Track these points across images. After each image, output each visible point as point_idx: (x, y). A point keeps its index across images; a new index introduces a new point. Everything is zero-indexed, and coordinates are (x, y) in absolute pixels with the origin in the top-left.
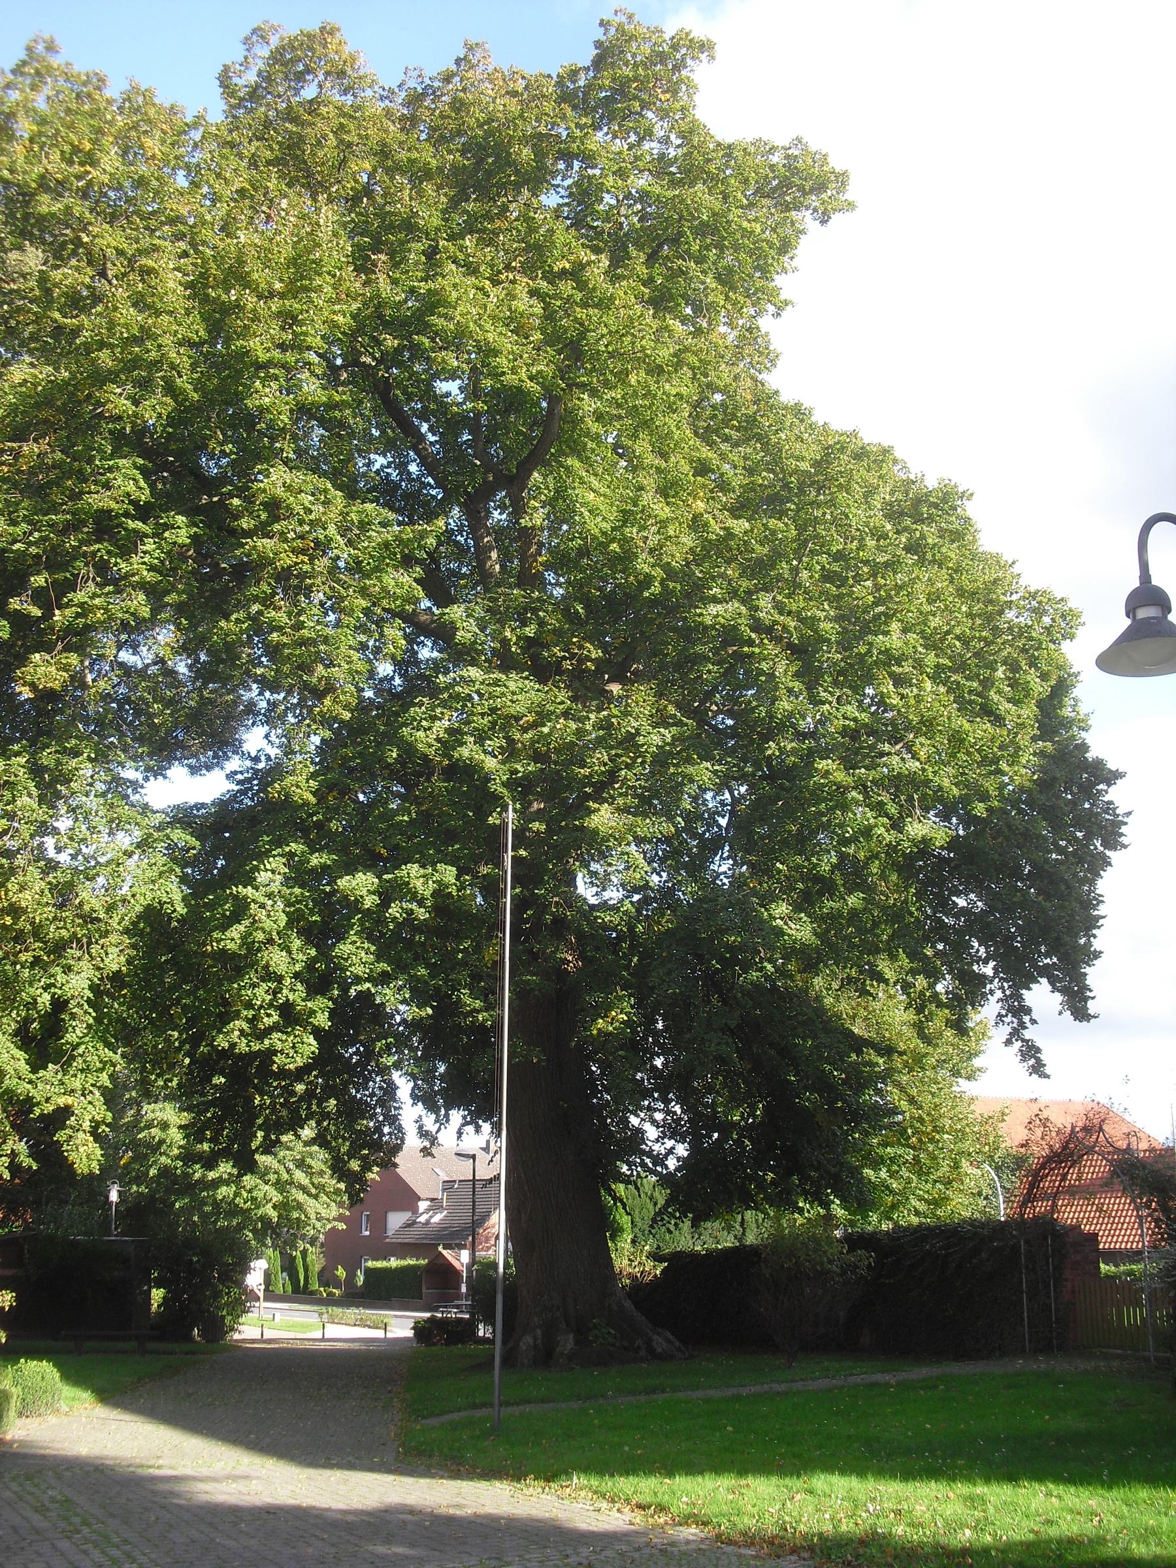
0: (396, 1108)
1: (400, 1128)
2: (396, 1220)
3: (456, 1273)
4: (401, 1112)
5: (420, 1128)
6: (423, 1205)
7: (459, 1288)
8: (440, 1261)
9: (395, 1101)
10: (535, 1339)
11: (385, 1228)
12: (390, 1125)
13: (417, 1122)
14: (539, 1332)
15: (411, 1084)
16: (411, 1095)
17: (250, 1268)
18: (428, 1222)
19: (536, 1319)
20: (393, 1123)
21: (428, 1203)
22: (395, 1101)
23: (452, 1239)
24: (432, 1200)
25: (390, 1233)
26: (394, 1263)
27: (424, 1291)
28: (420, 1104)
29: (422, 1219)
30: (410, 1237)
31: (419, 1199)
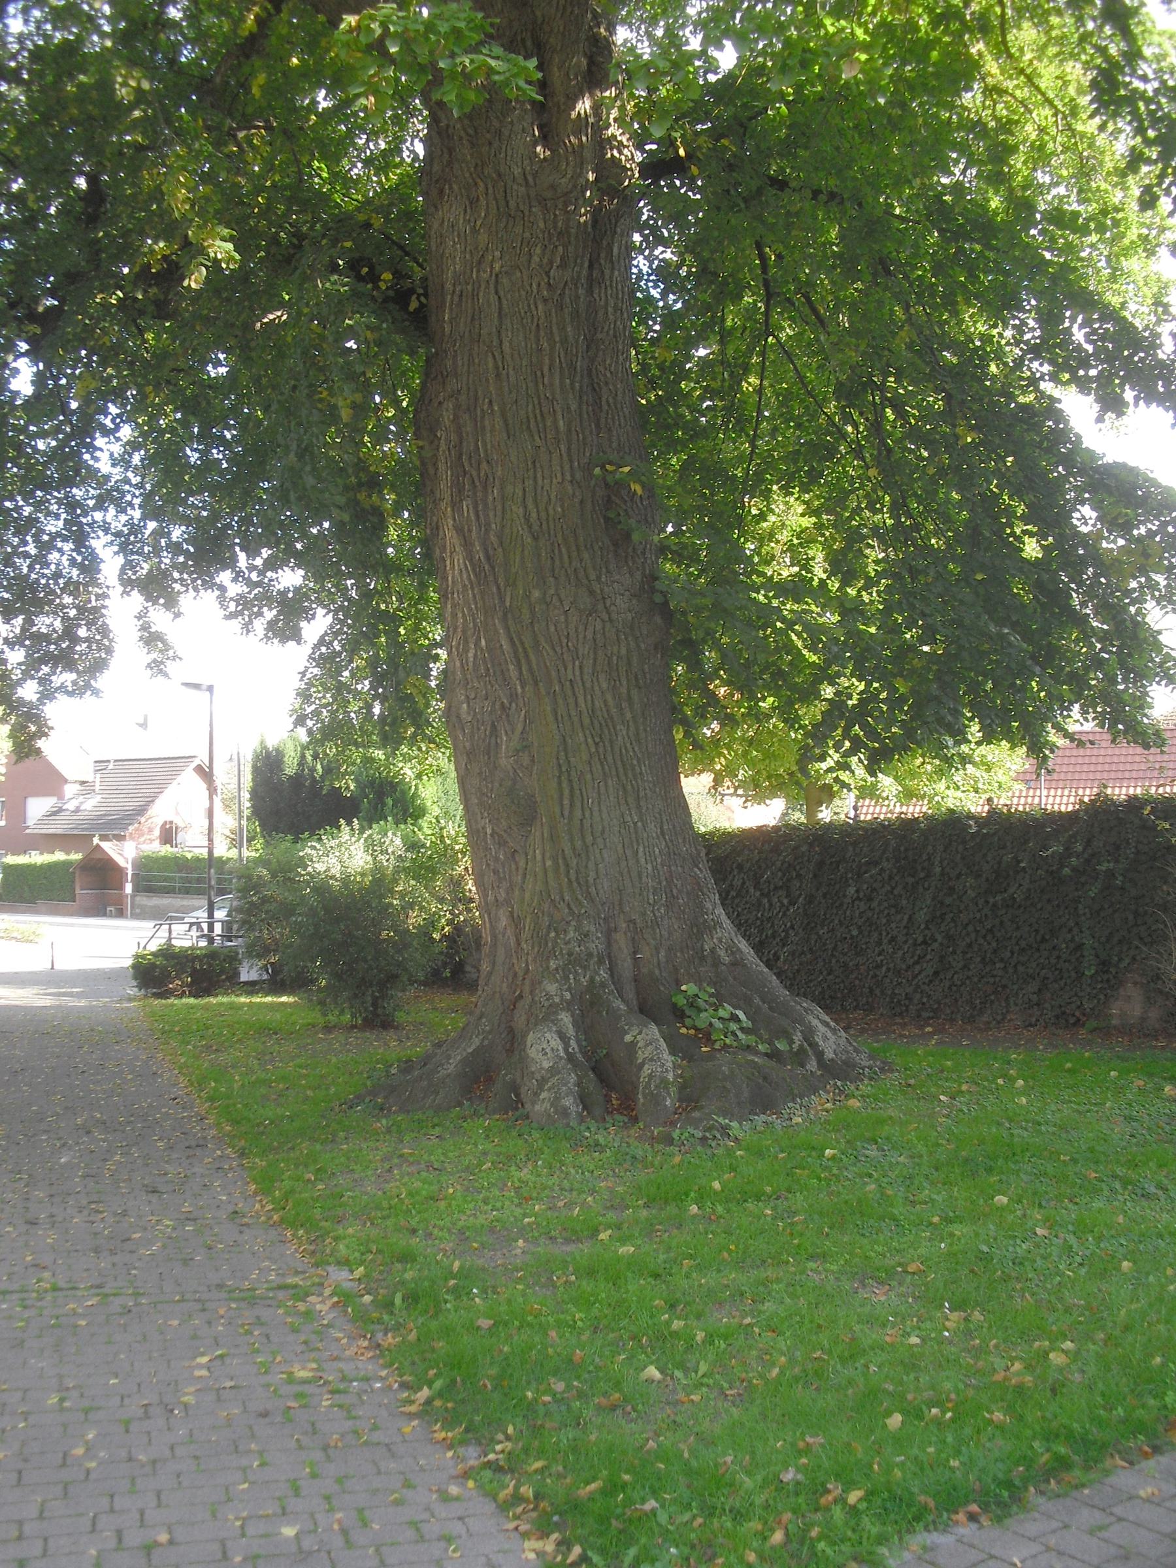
0: (98, 596)
1: (105, 631)
2: (37, 808)
3: (120, 871)
4: (107, 602)
5: (145, 627)
6: (70, 790)
7: (121, 887)
8: (98, 856)
9: (99, 586)
10: (562, 1036)
11: (24, 818)
12: (89, 625)
13: (139, 618)
14: (565, 1018)
15: (120, 560)
16: (121, 579)
17: (992, 812)
18: (77, 810)
19: (552, 988)
20: (94, 623)
21: (78, 787)
22: (99, 586)
23: (111, 829)
24: (83, 783)
25: (30, 822)
26: (37, 858)
27: (78, 891)
28: (135, 593)
29: (71, 806)
30: (58, 826)
31: (66, 781)
